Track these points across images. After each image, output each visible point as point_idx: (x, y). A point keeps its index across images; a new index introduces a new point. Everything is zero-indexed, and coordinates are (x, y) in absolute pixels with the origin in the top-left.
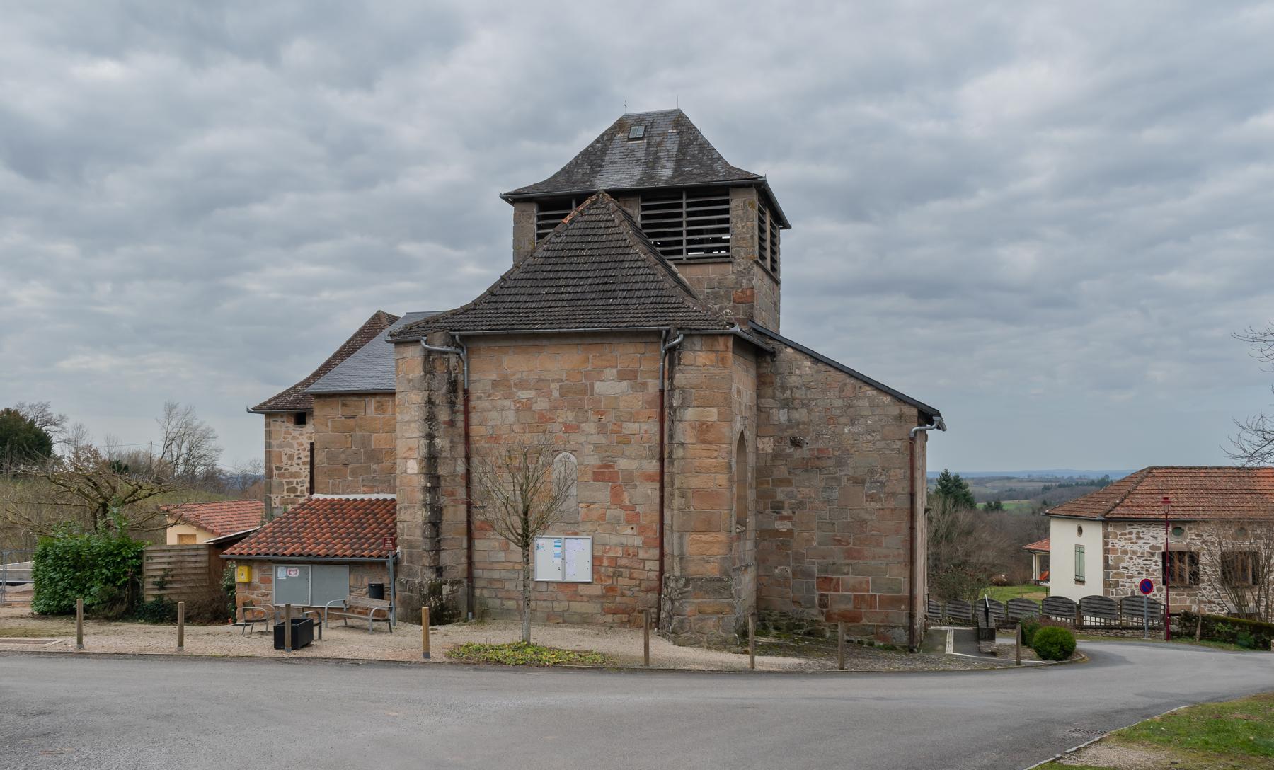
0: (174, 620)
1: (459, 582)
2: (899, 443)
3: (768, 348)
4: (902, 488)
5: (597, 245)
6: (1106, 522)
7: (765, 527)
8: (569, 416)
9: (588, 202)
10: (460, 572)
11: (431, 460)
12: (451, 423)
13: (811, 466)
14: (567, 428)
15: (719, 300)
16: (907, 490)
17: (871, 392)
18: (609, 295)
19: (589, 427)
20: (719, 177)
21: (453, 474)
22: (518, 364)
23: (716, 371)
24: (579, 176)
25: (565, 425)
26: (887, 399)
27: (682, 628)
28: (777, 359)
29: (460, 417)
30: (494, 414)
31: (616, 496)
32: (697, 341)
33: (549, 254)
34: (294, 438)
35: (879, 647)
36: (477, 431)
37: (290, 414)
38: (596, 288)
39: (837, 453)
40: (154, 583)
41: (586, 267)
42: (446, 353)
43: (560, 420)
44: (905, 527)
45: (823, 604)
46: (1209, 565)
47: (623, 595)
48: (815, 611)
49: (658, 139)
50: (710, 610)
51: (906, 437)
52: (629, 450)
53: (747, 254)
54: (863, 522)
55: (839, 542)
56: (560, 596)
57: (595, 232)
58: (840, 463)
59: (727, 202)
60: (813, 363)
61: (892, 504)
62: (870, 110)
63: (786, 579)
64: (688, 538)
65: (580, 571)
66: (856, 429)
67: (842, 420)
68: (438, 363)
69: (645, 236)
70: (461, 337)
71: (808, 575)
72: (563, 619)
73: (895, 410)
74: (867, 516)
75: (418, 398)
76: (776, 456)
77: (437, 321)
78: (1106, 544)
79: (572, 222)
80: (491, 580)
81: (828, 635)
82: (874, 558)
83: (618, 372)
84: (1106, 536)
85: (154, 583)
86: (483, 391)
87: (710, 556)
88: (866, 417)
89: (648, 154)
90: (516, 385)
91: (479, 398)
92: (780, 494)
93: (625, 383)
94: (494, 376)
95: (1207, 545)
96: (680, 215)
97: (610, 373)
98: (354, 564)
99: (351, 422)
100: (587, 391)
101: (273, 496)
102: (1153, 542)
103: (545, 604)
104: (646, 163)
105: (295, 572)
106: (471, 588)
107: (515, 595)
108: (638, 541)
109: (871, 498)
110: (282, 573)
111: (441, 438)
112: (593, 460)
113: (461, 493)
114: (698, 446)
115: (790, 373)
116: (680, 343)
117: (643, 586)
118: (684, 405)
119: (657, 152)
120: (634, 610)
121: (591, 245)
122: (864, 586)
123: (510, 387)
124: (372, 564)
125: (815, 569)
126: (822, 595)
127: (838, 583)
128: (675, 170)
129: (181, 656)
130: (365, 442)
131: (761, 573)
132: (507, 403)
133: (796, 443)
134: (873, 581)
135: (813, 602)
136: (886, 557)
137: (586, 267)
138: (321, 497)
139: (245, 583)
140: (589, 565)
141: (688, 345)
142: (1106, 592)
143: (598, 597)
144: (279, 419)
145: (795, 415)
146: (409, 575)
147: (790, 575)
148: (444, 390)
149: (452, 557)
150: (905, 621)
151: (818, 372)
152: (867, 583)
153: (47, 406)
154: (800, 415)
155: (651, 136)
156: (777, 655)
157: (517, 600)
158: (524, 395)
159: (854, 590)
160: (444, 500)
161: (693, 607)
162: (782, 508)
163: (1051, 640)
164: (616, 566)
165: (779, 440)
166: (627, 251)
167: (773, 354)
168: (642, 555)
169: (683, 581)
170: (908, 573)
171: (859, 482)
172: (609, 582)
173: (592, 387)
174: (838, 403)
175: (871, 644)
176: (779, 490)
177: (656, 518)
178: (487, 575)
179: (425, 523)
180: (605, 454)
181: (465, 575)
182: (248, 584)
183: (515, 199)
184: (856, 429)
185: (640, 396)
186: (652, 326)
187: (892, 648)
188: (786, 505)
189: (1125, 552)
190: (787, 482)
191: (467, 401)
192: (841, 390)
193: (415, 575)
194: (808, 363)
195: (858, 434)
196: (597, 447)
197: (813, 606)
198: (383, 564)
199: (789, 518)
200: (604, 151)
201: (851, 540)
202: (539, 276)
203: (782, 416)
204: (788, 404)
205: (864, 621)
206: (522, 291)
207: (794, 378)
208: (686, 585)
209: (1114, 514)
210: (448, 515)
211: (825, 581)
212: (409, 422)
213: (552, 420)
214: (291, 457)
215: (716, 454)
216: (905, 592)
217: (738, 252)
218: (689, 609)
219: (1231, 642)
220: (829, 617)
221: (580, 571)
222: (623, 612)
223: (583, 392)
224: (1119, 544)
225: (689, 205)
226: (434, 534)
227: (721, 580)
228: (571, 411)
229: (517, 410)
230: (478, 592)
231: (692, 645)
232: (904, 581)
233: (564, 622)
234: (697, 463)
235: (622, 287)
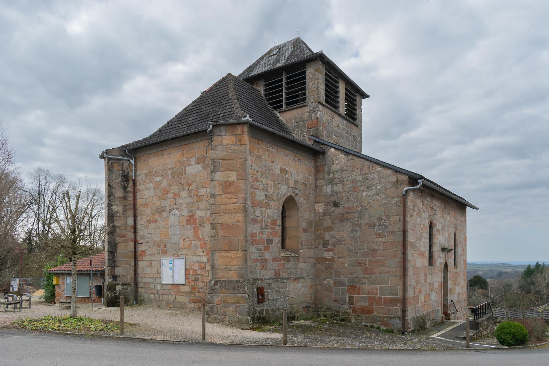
0: (118, 306)
1: (128, 284)
2: (396, 199)
3: (320, 150)
4: (398, 228)
7: (319, 256)
10: (129, 278)
12: (125, 198)
13: (343, 218)
15: (300, 129)
16: (401, 229)
17: (379, 169)
19: (184, 194)
23: (236, 147)
26: (389, 172)
27: (212, 311)
28: (326, 155)
32: (223, 129)
35: (383, 331)
36: (139, 202)
39: (359, 209)
42: (121, 160)
43: (172, 191)
44: (400, 252)
45: (351, 303)
47: (199, 292)
48: (346, 306)
51: (400, 195)
52: (202, 205)
53: (314, 100)
54: (374, 251)
58: (361, 215)
60: (345, 155)
61: (391, 238)
62: (529, 111)
63: (331, 287)
64: (217, 255)
65: (180, 279)
66: (370, 193)
67: (362, 188)
68: (115, 165)
71: (342, 284)
74: (376, 247)
76: (325, 214)
80: (145, 283)
81: (353, 321)
82: (381, 273)
83: (196, 159)
87: (232, 266)
88: (377, 184)
92: (327, 236)
93: (200, 165)
100: (182, 173)
109: (379, 235)
111: (117, 205)
112: (186, 213)
113: (131, 236)
114: (223, 196)
115: (333, 163)
122: (375, 291)
125: (346, 280)
126: (350, 297)
127: (359, 289)
131: (317, 283)
133: (336, 205)
134: (380, 288)
135: (345, 301)
136: (388, 272)
140: (184, 274)
141: (217, 131)
143: (188, 293)
145: (336, 188)
147: (333, 285)
148: (120, 179)
150: (400, 314)
151: (348, 160)
152: (377, 289)
154: (338, 188)
159: (369, 294)
160: (118, 240)
161: (220, 299)
162: (328, 244)
163: (506, 331)
164: (196, 275)
165: (327, 204)
167: (323, 153)
169: (213, 282)
170: (402, 283)
172: (193, 284)
174: (360, 178)
175: (378, 328)
176: (327, 234)
180: (191, 209)
181: (133, 280)
184: (370, 193)
187: (391, 331)
188: (330, 242)
190: (331, 229)
192: (362, 170)
194: (342, 156)
195: (371, 196)
196: (187, 204)
197: (345, 304)
199: (332, 250)
201: (367, 263)
203: (328, 189)
204: (331, 182)
205: (375, 313)
207: (335, 166)
210: (121, 248)
215: (235, 200)
216: (400, 296)
217: (310, 99)
218: (216, 300)
220: (354, 311)
221: (180, 279)
222: (200, 302)
226: (111, 258)
227: (238, 282)
229: (155, 188)
232: (400, 288)
234: (223, 207)
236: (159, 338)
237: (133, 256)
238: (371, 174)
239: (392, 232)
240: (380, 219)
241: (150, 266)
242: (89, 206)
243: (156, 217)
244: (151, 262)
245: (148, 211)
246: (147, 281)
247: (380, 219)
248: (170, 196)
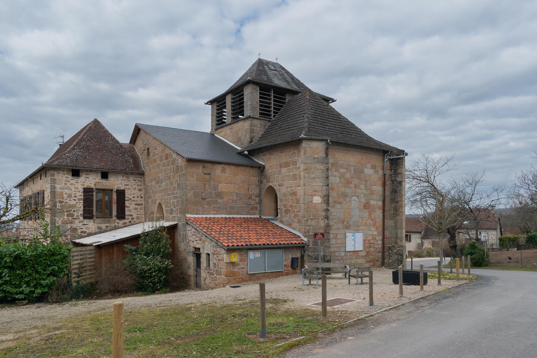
19: (362, 187)
25: (355, 185)
31: (370, 215)
34: (72, 184)
37: (68, 170)
52: (374, 197)
93: (373, 170)
99: (208, 177)
100: (362, 172)
101: (57, 219)
105: (258, 254)
108: (376, 233)
110: (252, 255)
112: (363, 200)
124: (239, 249)
130: (215, 188)
132: (336, 173)
144: (61, 173)
158: (343, 171)
168: (377, 239)
173: (364, 170)
196: (365, 195)
212: (314, 178)
213: (350, 183)
214: (70, 196)
221: (359, 247)
229: (340, 177)
244: (337, 234)
246: (333, 250)
248: (352, 186)
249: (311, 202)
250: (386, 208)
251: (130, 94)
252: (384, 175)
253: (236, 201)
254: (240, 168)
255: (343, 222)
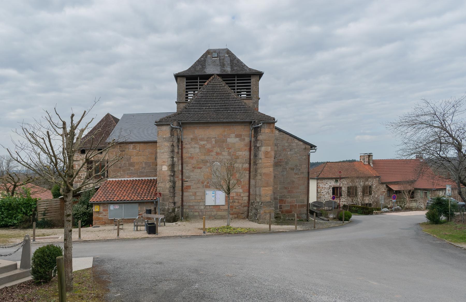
0: (32, 228)
5: (218, 93)
6: (317, 179)
8: (219, 150)
9: (211, 78)
10: (179, 204)
11: (172, 166)
12: (178, 153)
14: (217, 154)
16: (307, 171)
17: (296, 141)
18: (228, 109)
19: (225, 153)
20: (248, 72)
21: (178, 170)
22: (201, 132)
23: (270, 134)
24: (199, 69)
25: (217, 153)
26: (301, 143)
27: (260, 218)
29: (180, 151)
30: (192, 150)
32: (265, 125)
33: (202, 95)
36: (185, 155)
38: (222, 107)
40: (41, 214)
41: (217, 100)
45: (281, 208)
46: (344, 189)
47: (235, 208)
49: (223, 58)
50: (267, 212)
54: (293, 182)
55: (286, 188)
56: (214, 210)
57: (216, 88)
58: (287, 163)
59: (250, 80)
64: (262, 189)
67: (288, 150)
68: (175, 132)
69: (219, 89)
70: (182, 123)
72: (215, 218)
73: (304, 146)
74: (294, 180)
75: (168, 144)
77: (170, 117)
78: (317, 185)
79: (208, 84)
80: (189, 206)
84: (317, 183)
85: (41, 214)
86: (188, 142)
89: (220, 63)
90: (199, 139)
91: (186, 144)
93: (237, 139)
94: (192, 137)
95: (344, 185)
96: (234, 83)
97: (233, 135)
98: (141, 203)
100: (224, 141)
102: (330, 185)
103: (208, 213)
104: (221, 65)
105: (117, 207)
106: (182, 209)
107: (198, 210)
109: (296, 174)
110: (112, 207)
116: (261, 126)
117: (242, 206)
118: (262, 146)
119: (223, 62)
120: (239, 213)
121: (216, 93)
123: (197, 140)
128: (231, 68)
129: (119, 240)
132: (196, 145)
137: (217, 100)
138: (111, 179)
139: (97, 212)
142: (317, 200)
146: (163, 206)
148: (176, 141)
149: (178, 199)
153: (370, 156)
155: (220, 57)
156: (288, 224)
157: (199, 212)
158: (202, 143)
160: (176, 179)
166: (230, 95)
169: (260, 203)
171: (292, 169)
174: (286, 144)
177: (247, 183)
178: (188, 204)
179: (170, 187)
182: (98, 212)
183: (177, 77)
184: (291, 153)
185: (242, 143)
186: (248, 120)
189: (323, 188)
191: (182, 145)
193: (166, 205)
197: (277, 209)
198: (153, 202)
200: (205, 61)
202: (201, 103)
206: (196, 107)
208: (261, 204)
209: (320, 176)
211: (281, 201)
212: (163, 153)
213: (212, 151)
216: (306, 203)
218: (262, 212)
219: (357, 213)
220: (282, 212)
222: (236, 214)
223: (223, 142)
224: (321, 185)
225: (237, 80)
227: (270, 202)
228: (216, 148)
230: (184, 210)
231: (263, 223)
233: (215, 219)
235: (231, 107)
236: (281, 230)
237: (181, 189)
238: (293, 143)
239: (303, 172)
240: (296, 166)
241: (195, 194)
242: (175, 159)
243: (201, 166)
244: (195, 193)
245: (194, 161)
246: (191, 205)
247: (296, 166)
248: (214, 154)
249: (161, 170)
250: (251, 170)
251: (340, 32)
252: (251, 141)
253: (145, 168)
254: (148, 144)
255: (203, 183)
